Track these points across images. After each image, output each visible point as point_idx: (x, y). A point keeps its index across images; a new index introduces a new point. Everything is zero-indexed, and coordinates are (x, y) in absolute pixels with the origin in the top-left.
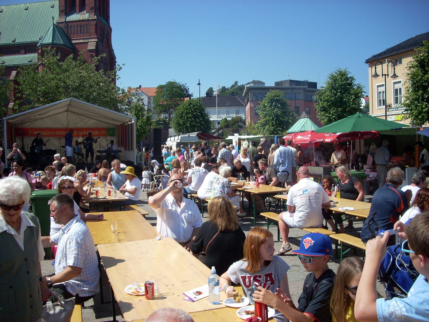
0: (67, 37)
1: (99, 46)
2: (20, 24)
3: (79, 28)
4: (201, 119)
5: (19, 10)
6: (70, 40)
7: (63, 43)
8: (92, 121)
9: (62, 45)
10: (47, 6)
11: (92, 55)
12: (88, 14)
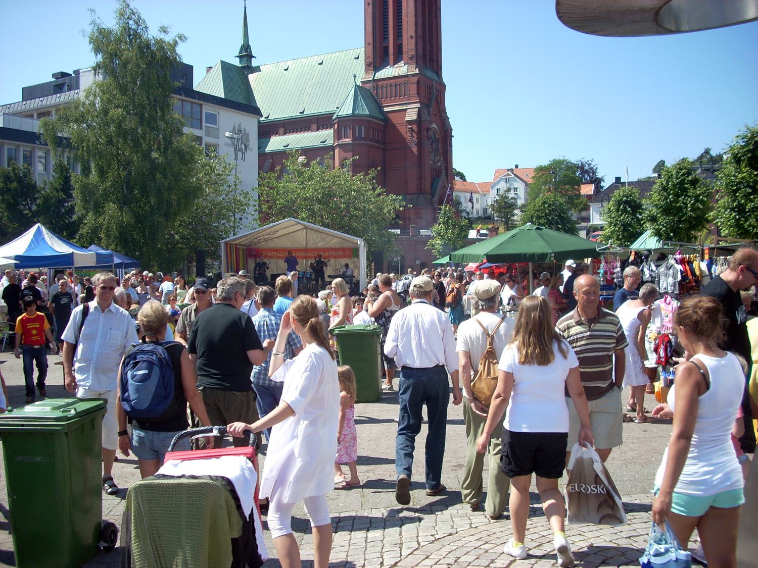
0: (377, 103)
1: (422, 115)
2: (312, 86)
4: (560, 226)
5: (310, 65)
6: (380, 108)
7: (368, 113)
8: (336, 239)
10: (350, 56)
11: (411, 128)
12: (406, 66)
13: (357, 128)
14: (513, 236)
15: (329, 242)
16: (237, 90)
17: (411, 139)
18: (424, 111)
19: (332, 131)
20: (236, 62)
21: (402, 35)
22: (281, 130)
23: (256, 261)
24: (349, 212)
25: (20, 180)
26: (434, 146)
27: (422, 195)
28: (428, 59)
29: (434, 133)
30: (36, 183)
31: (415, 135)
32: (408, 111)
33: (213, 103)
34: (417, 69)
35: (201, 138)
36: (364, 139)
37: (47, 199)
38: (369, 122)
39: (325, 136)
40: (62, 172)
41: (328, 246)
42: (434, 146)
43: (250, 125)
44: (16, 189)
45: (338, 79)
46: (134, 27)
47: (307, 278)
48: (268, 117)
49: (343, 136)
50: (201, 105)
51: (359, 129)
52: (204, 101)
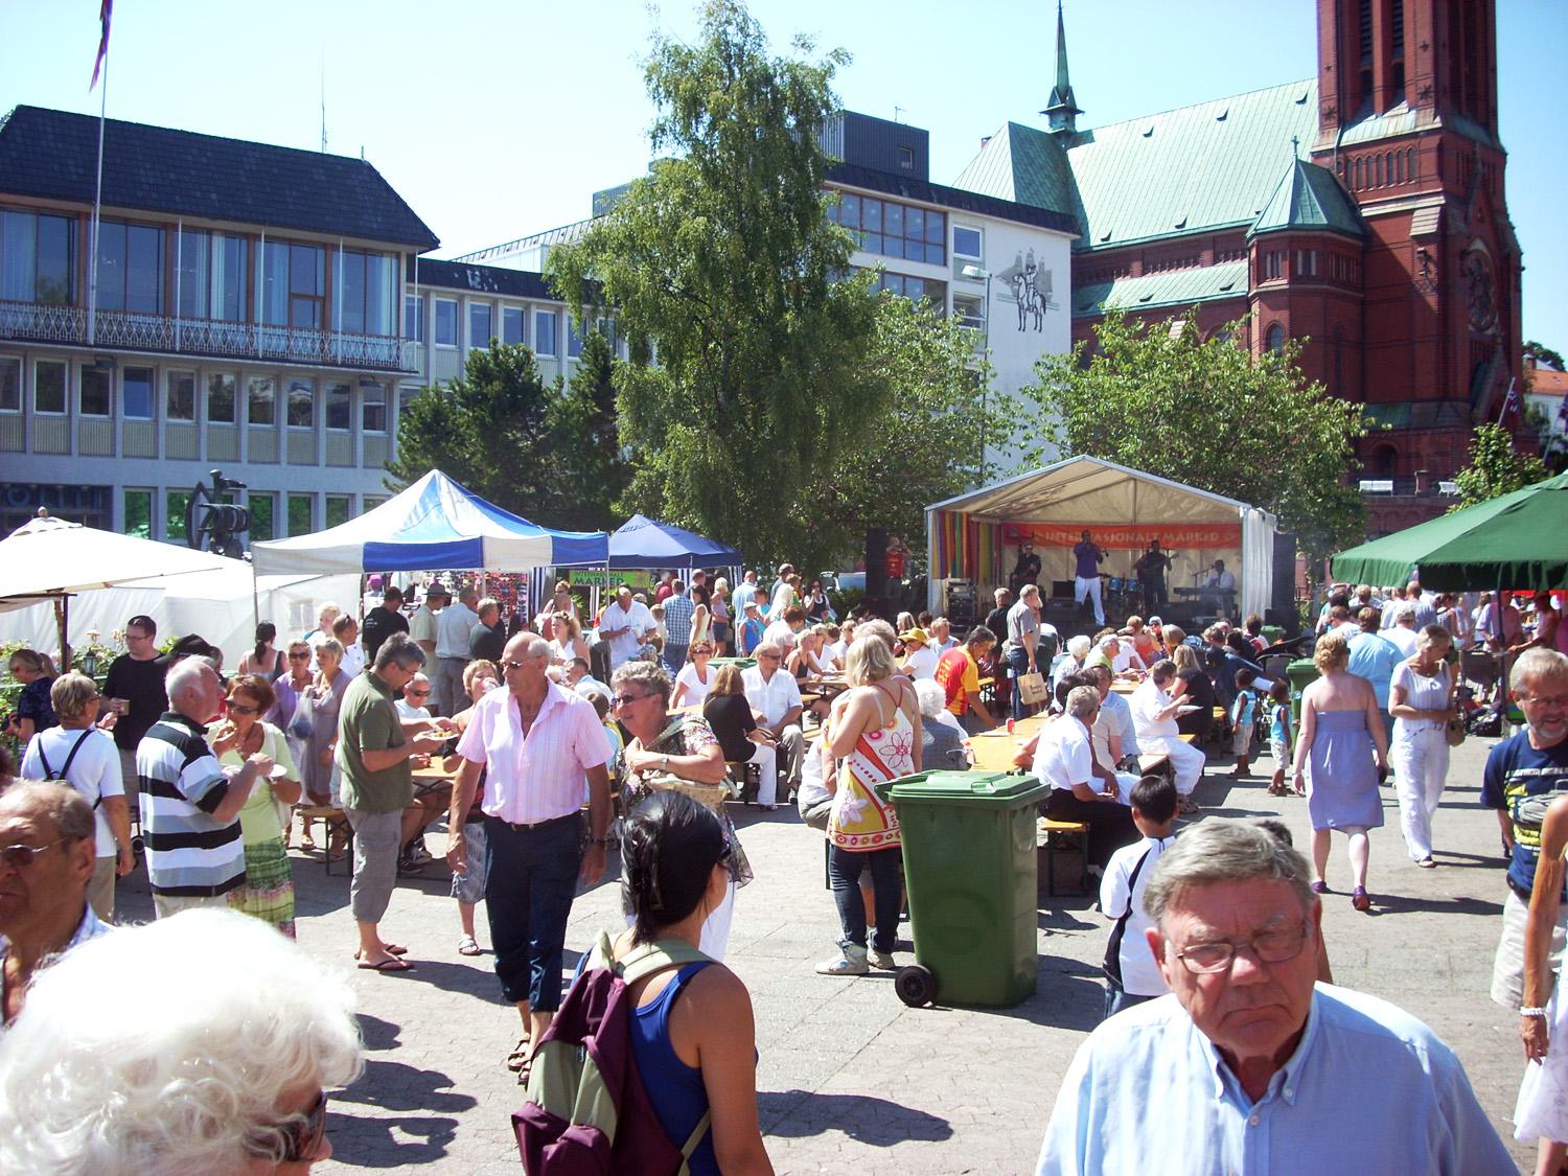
1: (1450, 221)
3: (1385, 164)
6: (1354, 209)
7: (1325, 222)
9: (1321, 228)
11: (1424, 252)
12: (1413, 112)
13: (1300, 254)
14: (1514, 509)
15: (1188, 509)
16: (1042, 184)
17: (1423, 276)
18: (1455, 211)
19: (1244, 264)
20: (1043, 125)
21: (1402, 45)
22: (1136, 266)
23: (1020, 551)
24: (1238, 440)
25: (509, 377)
26: (1479, 291)
27: (1447, 404)
28: (1463, 95)
29: (1478, 261)
30: (540, 381)
31: (1432, 267)
32: (1416, 213)
33: (971, 209)
34: (1438, 119)
35: (945, 284)
36: (1313, 280)
37: (565, 412)
38: (1325, 241)
39: (1230, 276)
40: (596, 358)
41: (1183, 519)
42: (1479, 291)
43: (1054, 253)
44: (498, 396)
45: (1261, 149)
46: (737, 39)
47: (1130, 593)
48: (1108, 239)
49: (1269, 274)
50: (945, 215)
51: (1304, 258)
52: (950, 204)
